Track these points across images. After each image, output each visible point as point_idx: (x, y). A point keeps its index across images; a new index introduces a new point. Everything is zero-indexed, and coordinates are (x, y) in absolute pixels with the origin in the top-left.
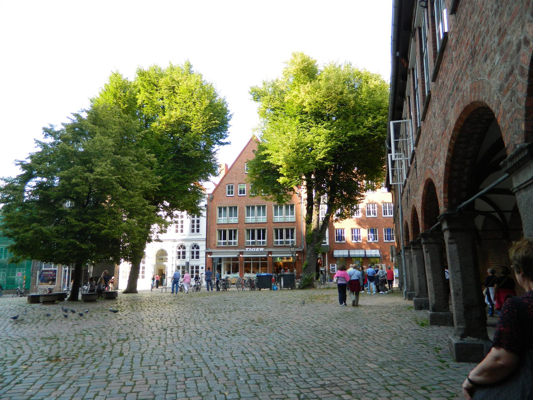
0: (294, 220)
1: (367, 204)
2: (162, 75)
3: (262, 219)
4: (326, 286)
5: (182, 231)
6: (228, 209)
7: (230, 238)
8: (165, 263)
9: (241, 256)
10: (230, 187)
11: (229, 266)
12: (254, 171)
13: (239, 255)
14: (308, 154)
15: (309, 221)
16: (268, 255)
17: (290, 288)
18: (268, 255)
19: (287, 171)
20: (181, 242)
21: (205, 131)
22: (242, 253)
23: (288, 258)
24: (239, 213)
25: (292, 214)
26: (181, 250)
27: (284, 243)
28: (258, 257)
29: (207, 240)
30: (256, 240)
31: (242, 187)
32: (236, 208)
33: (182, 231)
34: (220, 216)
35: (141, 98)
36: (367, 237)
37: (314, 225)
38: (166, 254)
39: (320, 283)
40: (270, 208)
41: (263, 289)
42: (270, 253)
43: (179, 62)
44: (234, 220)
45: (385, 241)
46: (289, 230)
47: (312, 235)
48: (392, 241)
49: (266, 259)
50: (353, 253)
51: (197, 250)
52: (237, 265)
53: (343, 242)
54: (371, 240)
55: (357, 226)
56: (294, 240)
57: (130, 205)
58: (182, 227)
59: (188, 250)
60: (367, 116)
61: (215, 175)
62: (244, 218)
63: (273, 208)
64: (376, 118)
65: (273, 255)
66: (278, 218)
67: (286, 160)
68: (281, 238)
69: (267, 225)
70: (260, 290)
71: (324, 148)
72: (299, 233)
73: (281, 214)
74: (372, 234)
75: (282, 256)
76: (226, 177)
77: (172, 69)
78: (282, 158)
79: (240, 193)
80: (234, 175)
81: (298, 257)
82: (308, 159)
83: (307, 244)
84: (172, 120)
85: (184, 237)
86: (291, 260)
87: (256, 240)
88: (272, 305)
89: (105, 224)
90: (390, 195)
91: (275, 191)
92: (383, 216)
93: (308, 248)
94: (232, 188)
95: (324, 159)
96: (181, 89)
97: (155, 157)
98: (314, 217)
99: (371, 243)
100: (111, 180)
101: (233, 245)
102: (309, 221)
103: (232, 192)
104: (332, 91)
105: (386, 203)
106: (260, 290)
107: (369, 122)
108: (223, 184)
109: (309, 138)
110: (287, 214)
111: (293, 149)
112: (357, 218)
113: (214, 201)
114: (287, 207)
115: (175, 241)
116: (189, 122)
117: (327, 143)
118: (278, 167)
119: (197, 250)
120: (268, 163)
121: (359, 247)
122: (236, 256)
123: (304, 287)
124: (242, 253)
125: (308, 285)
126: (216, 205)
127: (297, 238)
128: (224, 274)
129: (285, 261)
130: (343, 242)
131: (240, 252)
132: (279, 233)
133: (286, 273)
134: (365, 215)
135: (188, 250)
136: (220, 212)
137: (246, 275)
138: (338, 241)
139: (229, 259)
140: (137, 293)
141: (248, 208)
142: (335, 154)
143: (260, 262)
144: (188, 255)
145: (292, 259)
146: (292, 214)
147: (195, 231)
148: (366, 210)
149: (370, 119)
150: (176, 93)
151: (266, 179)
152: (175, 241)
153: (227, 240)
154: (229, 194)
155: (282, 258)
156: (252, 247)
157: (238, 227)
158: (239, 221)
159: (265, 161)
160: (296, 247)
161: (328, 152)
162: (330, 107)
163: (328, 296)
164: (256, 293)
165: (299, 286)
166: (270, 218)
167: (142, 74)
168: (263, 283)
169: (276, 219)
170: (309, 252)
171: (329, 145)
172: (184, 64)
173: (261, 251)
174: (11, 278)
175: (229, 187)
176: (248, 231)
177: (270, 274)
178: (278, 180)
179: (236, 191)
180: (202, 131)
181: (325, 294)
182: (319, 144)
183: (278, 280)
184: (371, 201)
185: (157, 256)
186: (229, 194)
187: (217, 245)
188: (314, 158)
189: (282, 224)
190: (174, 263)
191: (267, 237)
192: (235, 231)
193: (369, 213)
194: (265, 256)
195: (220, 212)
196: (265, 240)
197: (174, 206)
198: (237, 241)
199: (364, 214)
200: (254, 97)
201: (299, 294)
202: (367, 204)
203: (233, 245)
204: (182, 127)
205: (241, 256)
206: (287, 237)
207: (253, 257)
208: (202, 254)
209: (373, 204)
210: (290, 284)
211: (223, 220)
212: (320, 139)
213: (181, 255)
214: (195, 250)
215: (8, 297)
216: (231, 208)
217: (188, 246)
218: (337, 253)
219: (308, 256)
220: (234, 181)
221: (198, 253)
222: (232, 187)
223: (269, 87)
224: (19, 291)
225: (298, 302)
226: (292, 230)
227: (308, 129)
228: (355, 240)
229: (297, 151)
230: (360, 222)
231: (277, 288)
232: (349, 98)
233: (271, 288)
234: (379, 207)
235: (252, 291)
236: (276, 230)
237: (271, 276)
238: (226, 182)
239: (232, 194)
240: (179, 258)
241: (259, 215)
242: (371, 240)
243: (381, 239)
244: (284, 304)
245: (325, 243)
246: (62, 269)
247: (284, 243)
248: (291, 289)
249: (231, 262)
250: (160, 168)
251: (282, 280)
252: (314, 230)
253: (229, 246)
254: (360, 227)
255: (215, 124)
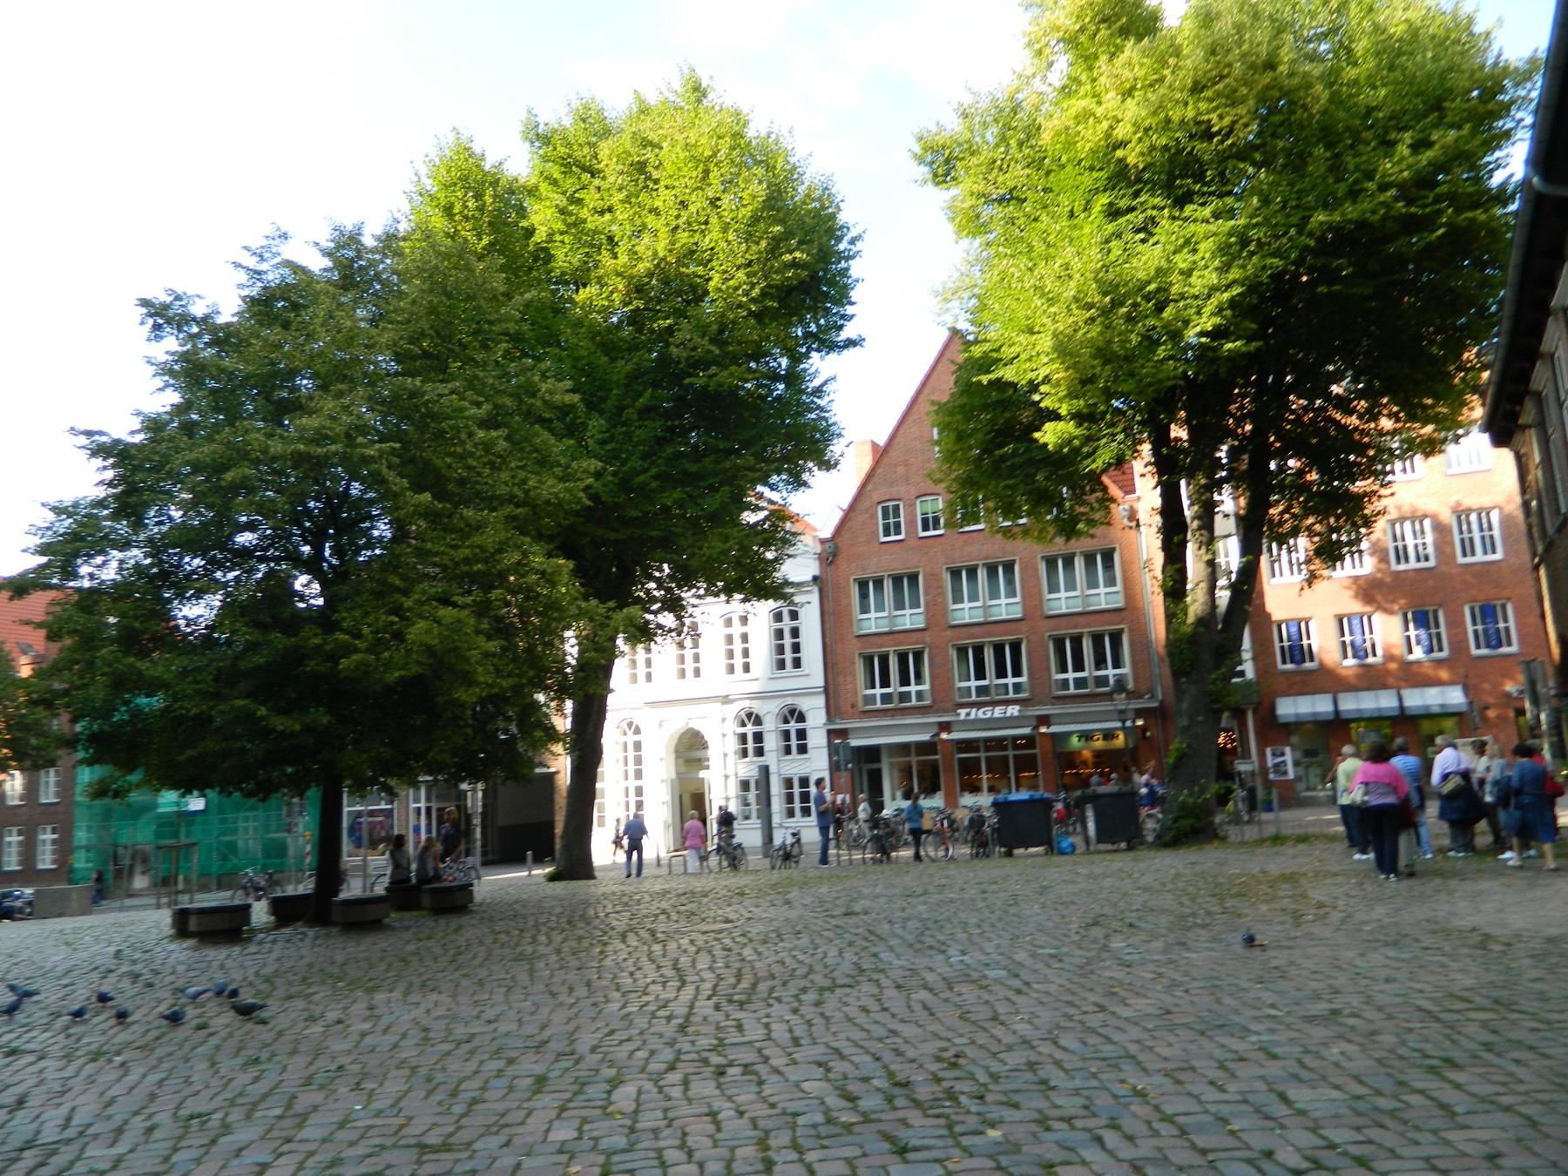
0: (1119, 602)
1: (1393, 523)
2: (606, 133)
3: (1007, 607)
4: (1270, 830)
5: (747, 668)
6: (888, 585)
7: (905, 681)
8: (702, 774)
9: (944, 736)
10: (891, 512)
11: (906, 772)
12: (961, 437)
13: (937, 734)
14: (1151, 322)
15: (1175, 590)
16: (1036, 728)
17: (1123, 845)
18: (1036, 728)
19: (1072, 395)
20: (746, 704)
21: (756, 292)
22: (946, 727)
23: (1109, 735)
24: (926, 594)
25: (1111, 582)
26: (750, 729)
27: (1091, 683)
28: (1004, 738)
29: (828, 691)
30: (991, 679)
31: (929, 508)
32: (913, 578)
33: (747, 668)
34: (865, 609)
35: (542, 218)
36: (1403, 642)
37: (1195, 602)
38: (705, 746)
39: (1236, 820)
40: (1030, 569)
41: (1021, 851)
42: (1044, 720)
43: (662, 83)
44: (911, 618)
45: (1474, 652)
46: (1106, 636)
47: (1193, 640)
48: (1505, 650)
49: (1030, 741)
50: (1350, 704)
51: (801, 726)
52: (934, 767)
53: (1308, 665)
54: (1418, 653)
55: (1357, 607)
56: (1126, 670)
57: (467, 561)
58: (746, 653)
59: (771, 727)
60: (1388, 145)
61: (828, 465)
62: (945, 606)
63: (1043, 567)
64: (1429, 144)
65: (1054, 729)
66: (1063, 601)
67: (1063, 350)
68: (1079, 667)
69: (1024, 626)
70: (1009, 854)
71: (1214, 289)
72: (1142, 642)
73: (1071, 586)
74: (1422, 633)
75: (1087, 730)
76: (874, 480)
77: (644, 110)
78: (1045, 342)
79: (926, 528)
80: (901, 470)
81: (1144, 729)
82: (1150, 342)
83: (1177, 674)
84: (642, 267)
85: (755, 687)
86: (1120, 741)
87: (991, 679)
88: (1041, 939)
89: (358, 636)
90: (1506, 456)
91: (1043, 499)
92: (1461, 560)
93: (1179, 692)
94: (897, 515)
95: (1218, 334)
96: (671, 156)
97: (573, 391)
98: (1194, 565)
99: (1418, 662)
100: (432, 494)
101: (914, 702)
102: (1175, 590)
103: (898, 525)
104: (1230, 57)
105: (1469, 511)
106: (1009, 854)
107: (1400, 163)
108: (865, 505)
109: (1147, 260)
110: (1092, 584)
111: (1090, 306)
112: (1356, 578)
113: (841, 561)
114: (1090, 559)
115: (726, 700)
116: (700, 270)
117: (1224, 269)
118: (1034, 387)
119: (801, 726)
120: (999, 384)
121: (1372, 678)
122: (925, 737)
123: (1173, 839)
124: (946, 727)
125: (1191, 829)
126: (850, 574)
127: (1134, 664)
128: (894, 799)
129: (1099, 744)
130: (1308, 665)
131: (940, 724)
132: (1067, 647)
133: (1102, 789)
134: (1388, 562)
135: (771, 727)
136: (864, 596)
137: (968, 800)
138: (1290, 666)
139: (904, 748)
140: (593, 877)
141: (955, 573)
142: (1258, 307)
143: (1010, 753)
144: (772, 742)
145: (1121, 737)
146: (1111, 582)
147: (789, 663)
148: (1391, 545)
149: (1403, 150)
150: (656, 182)
151: (1003, 458)
152: (726, 700)
153: (895, 688)
154: (887, 533)
155: (1087, 736)
156: (978, 705)
157: (928, 639)
158: (928, 621)
159: (985, 379)
160: (1132, 695)
161: (1233, 303)
162: (1227, 121)
163: (1290, 878)
164: (996, 868)
165: (1159, 837)
166: (1032, 601)
167: (542, 138)
168: (1017, 830)
169: (1055, 604)
170: (1184, 706)
171: (1235, 274)
172: (677, 86)
173: (1012, 717)
174: (273, 840)
175: (885, 510)
176: (962, 651)
177: (1036, 798)
178: (1036, 435)
179: (911, 522)
180: (746, 294)
181: (1274, 868)
182: (1193, 280)
183: (1074, 812)
184: (1406, 509)
185: (678, 752)
186: (887, 533)
187: (861, 706)
188: (1175, 336)
189: (1074, 620)
190: (731, 772)
191: (1029, 668)
192: (918, 656)
193: (1402, 555)
194: (1027, 731)
195: (864, 596)
196: (1023, 679)
197: (685, 577)
198: (926, 687)
199: (1384, 559)
200: (935, 175)
201: (1157, 872)
202: (1393, 523)
203: (914, 702)
204: (674, 288)
205: (944, 736)
206: (1100, 662)
207: (987, 740)
208: (817, 739)
209: (1417, 518)
210: (1120, 827)
211: (873, 621)
212: (1195, 263)
213: (751, 744)
214: (793, 726)
215: (129, 908)
216: (897, 580)
217: (770, 712)
218: (1290, 708)
219: (1184, 722)
220: (901, 490)
221: (802, 734)
222: (896, 508)
223: (985, 125)
224: (251, 880)
225: (1164, 920)
226: (1116, 638)
227: (1146, 229)
228: (1354, 656)
229: (1106, 312)
230: (1369, 591)
231: (1073, 846)
232: (1306, 74)
233: (1052, 849)
234: (1440, 529)
235: (980, 863)
236: (1059, 643)
237: (1047, 804)
238: (876, 497)
239: (898, 533)
240: (745, 754)
241: (994, 594)
242: (1418, 653)
243: (1459, 647)
244: (1097, 932)
245: (1242, 674)
246: (407, 806)
247: (1091, 683)
248: (1130, 848)
249: (914, 760)
250: (611, 440)
251: (1090, 814)
252: (1200, 621)
253: (899, 707)
254: (1368, 609)
255: (794, 264)
